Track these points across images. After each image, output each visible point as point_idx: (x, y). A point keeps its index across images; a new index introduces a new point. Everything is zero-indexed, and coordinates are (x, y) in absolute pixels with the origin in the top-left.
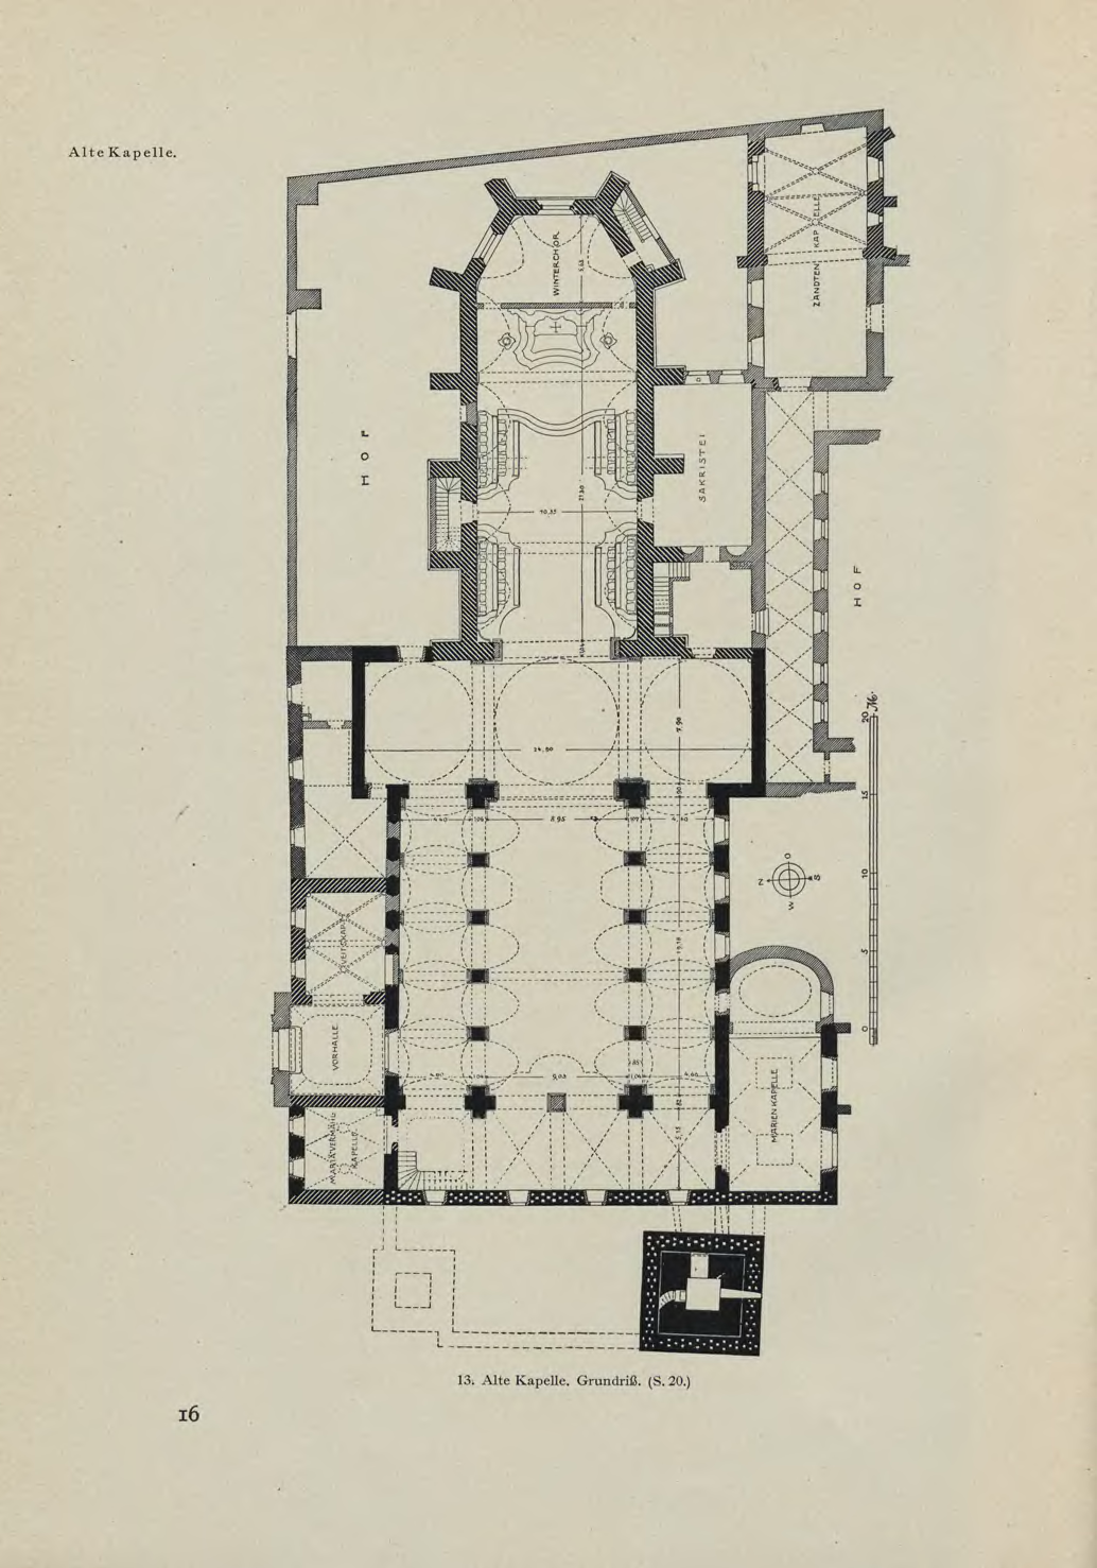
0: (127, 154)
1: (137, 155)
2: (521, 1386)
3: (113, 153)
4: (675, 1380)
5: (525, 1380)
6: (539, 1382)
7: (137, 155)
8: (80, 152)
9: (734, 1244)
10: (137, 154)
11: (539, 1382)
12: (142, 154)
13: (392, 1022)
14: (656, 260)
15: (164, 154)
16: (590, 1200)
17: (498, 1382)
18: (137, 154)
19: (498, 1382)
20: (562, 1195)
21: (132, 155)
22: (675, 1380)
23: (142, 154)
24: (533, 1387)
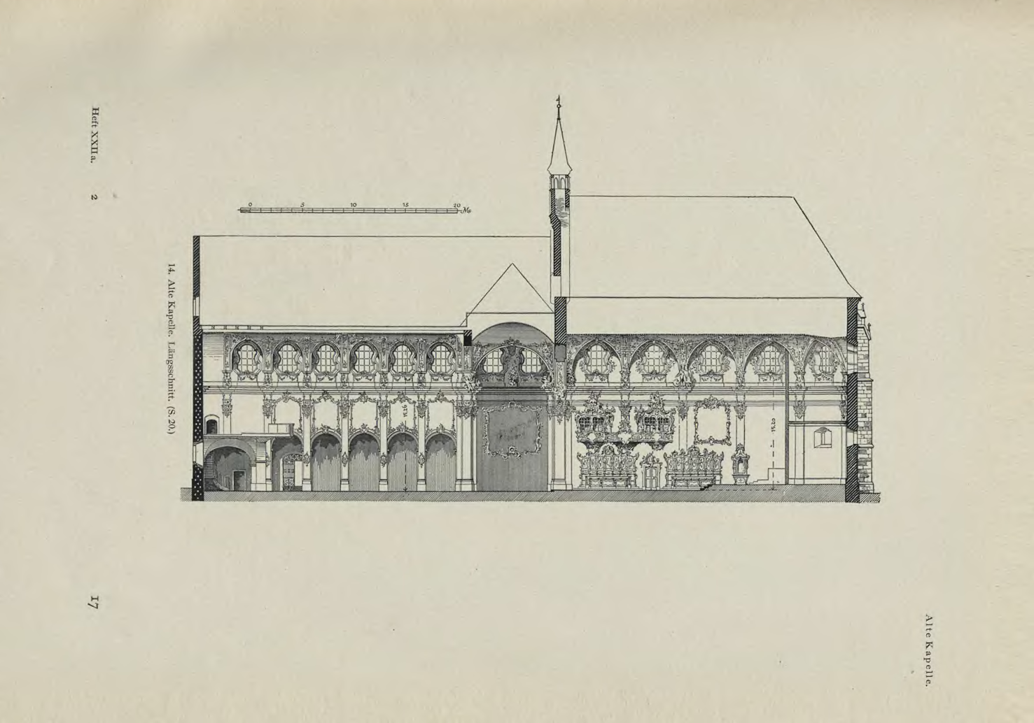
0: (928, 654)
1: (928, 660)
2: (167, 305)
3: (929, 644)
4: (172, 424)
5: (172, 308)
6: (171, 317)
7: (928, 660)
8: (928, 622)
9: (198, 410)
10: (928, 660)
11: (171, 317)
12: (928, 664)
13: (242, 211)
14: (828, 441)
15: (929, 678)
16: (197, 445)
17: (171, 290)
18: (928, 660)
19: (171, 290)
20: (200, 403)
21: (928, 657)
22: (172, 424)
23: (928, 664)
24: (167, 313)
